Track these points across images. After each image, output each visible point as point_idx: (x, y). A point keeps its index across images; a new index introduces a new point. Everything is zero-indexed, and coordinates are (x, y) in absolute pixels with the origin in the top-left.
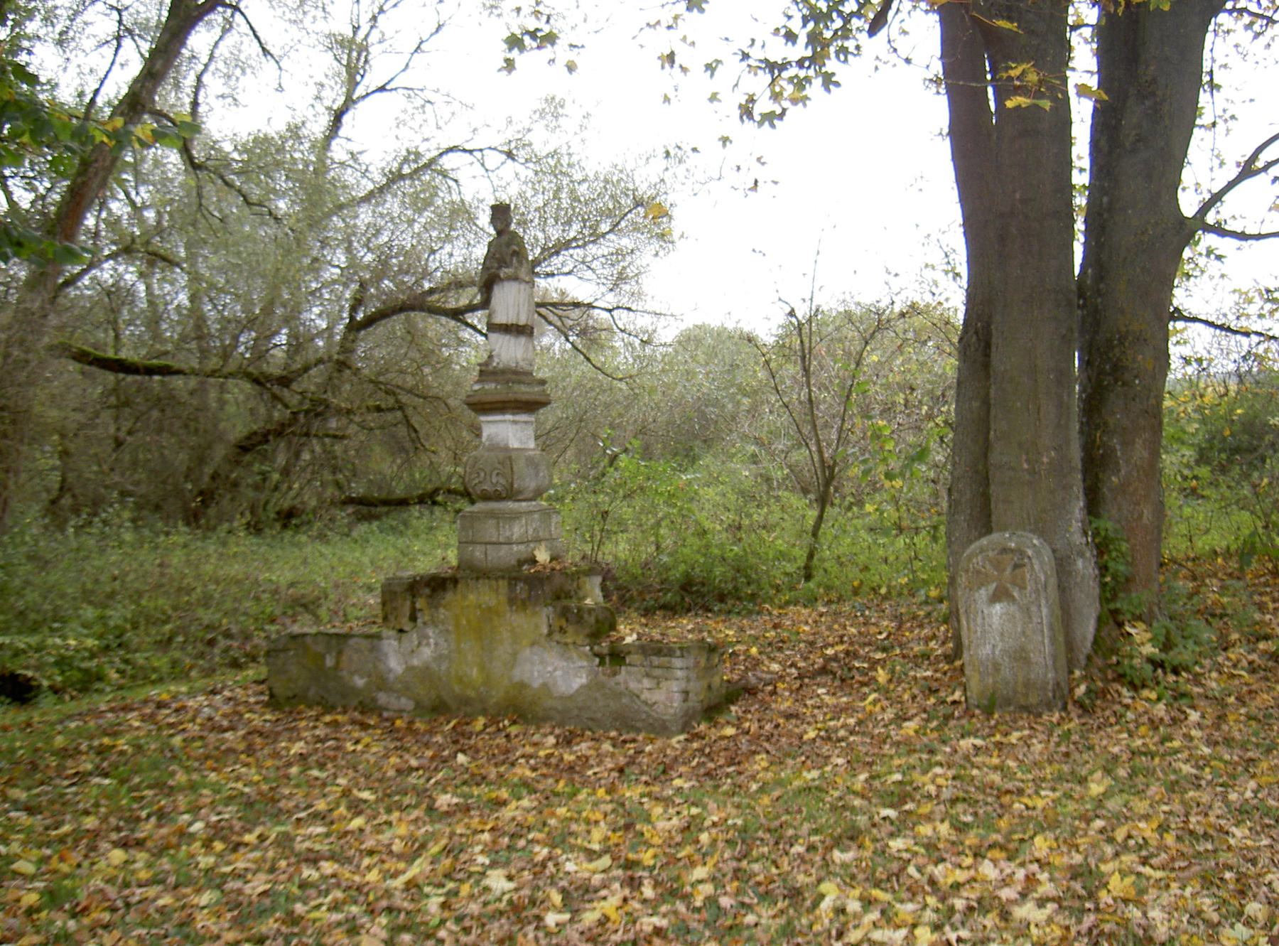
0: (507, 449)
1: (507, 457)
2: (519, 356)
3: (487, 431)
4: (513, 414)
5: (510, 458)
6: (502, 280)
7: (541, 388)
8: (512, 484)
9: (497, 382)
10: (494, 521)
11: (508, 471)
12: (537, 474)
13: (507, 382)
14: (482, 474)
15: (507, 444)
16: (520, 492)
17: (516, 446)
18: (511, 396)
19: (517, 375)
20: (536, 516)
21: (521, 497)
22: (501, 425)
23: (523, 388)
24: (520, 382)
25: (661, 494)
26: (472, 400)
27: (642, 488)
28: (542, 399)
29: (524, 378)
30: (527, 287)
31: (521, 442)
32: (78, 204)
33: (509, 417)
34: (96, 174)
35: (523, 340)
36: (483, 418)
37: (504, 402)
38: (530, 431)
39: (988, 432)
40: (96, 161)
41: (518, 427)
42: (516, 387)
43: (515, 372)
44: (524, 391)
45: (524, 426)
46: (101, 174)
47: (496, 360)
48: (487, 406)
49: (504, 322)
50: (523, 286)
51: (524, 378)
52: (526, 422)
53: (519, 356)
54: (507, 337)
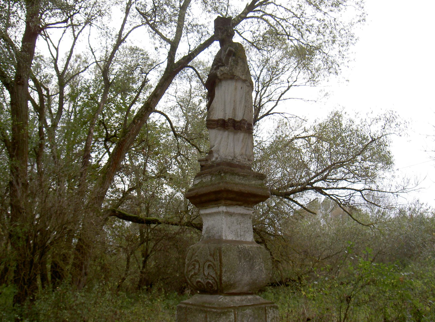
0: (220, 241)
1: (218, 249)
2: (238, 151)
3: (207, 223)
4: (226, 205)
5: (220, 250)
6: (220, 80)
7: (260, 182)
8: (221, 276)
9: (211, 174)
10: (203, 315)
11: (217, 263)
12: (252, 267)
13: (220, 173)
14: (197, 267)
15: (220, 236)
16: (232, 286)
17: (230, 237)
18: (222, 186)
19: (230, 167)
20: (248, 311)
21: (234, 291)
22: (218, 218)
23: (237, 180)
24: (233, 174)
25: (387, 285)
26: (193, 193)
27: (373, 281)
28: (260, 192)
29: (237, 170)
30: (245, 86)
31: (237, 235)
32: (121, 149)
33: (223, 209)
34: (129, 136)
35: (241, 136)
36: (202, 212)
37: (216, 193)
38: (249, 225)
39: (251, 294)
40: (129, 131)
41: (234, 219)
42: (228, 178)
43: (230, 164)
44: (237, 183)
45: (240, 219)
46: (131, 136)
47: (215, 155)
48: (204, 199)
49: (221, 117)
50: (239, 85)
51: (237, 170)
52: (243, 215)
53: (238, 151)
54: (226, 133)
